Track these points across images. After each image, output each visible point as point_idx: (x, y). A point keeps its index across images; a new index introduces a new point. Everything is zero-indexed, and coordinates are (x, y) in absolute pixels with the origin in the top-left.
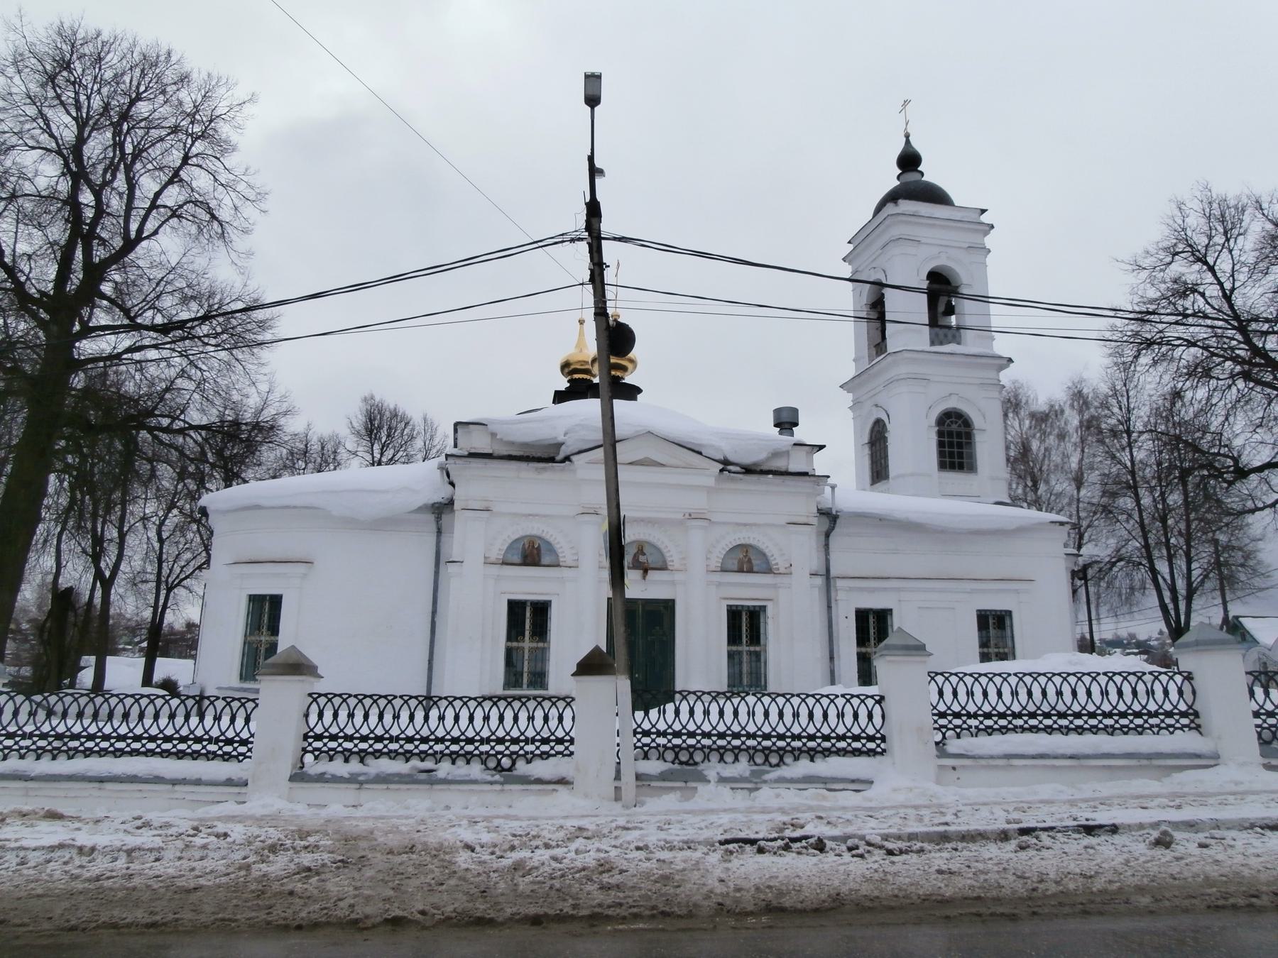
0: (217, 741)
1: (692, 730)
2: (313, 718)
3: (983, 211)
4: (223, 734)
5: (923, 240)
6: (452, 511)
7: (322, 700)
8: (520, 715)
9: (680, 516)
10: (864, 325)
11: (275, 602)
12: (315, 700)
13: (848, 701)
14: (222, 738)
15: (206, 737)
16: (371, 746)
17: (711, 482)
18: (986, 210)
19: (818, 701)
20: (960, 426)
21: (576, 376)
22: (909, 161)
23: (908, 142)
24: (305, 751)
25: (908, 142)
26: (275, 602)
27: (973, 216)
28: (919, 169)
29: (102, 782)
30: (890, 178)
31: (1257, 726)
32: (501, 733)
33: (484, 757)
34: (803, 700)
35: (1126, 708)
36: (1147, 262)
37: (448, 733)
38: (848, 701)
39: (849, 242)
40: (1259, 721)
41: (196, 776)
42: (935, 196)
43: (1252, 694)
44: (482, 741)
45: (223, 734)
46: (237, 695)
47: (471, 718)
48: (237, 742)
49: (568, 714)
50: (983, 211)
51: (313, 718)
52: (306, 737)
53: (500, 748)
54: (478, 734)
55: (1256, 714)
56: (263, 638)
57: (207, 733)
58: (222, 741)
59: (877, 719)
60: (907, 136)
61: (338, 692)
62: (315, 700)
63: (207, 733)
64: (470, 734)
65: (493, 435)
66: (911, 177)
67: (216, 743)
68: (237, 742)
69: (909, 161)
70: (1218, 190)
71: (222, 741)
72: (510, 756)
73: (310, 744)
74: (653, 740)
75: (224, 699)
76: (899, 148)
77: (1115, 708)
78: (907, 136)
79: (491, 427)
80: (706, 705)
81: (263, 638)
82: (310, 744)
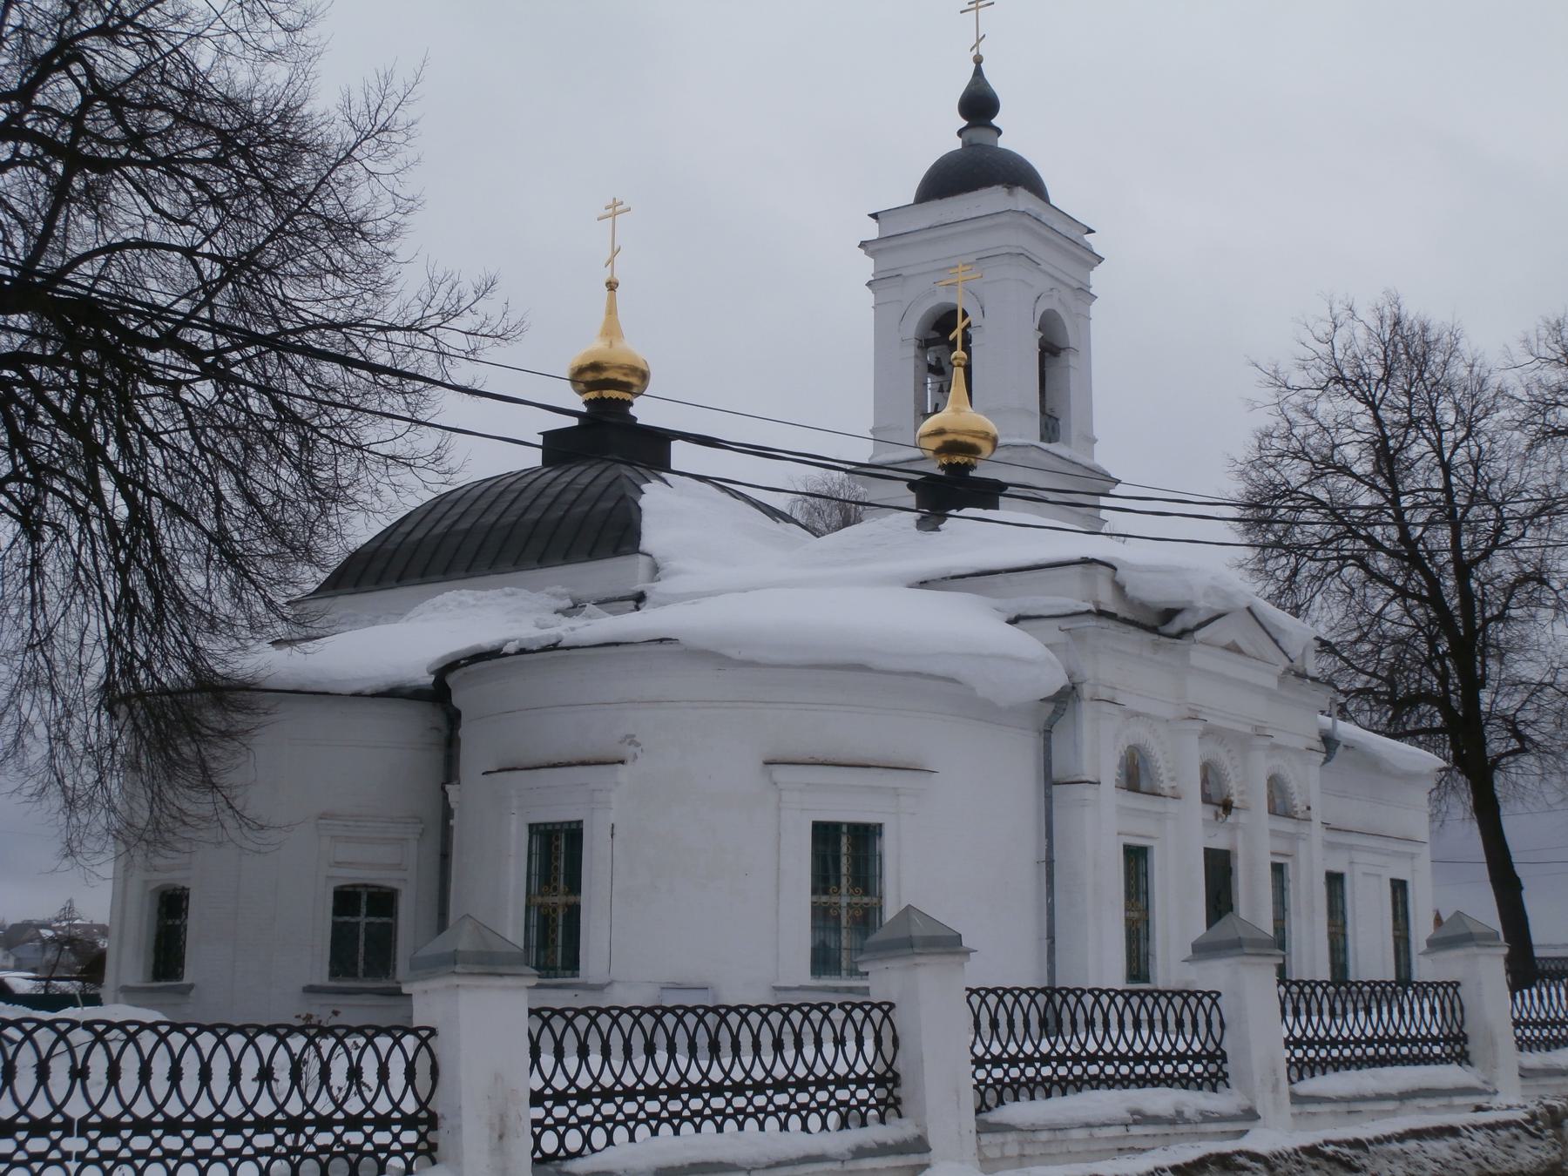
0: (84, 1127)
1: (325, 1113)
3: (1090, 231)
4: (95, 1110)
5: (1044, 266)
6: (1078, 698)
8: (333, 1065)
9: (1248, 730)
11: (865, 836)
14: (95, 1119)
15: (57, 1119)
17: (1271, 682)
18: (1093, 232)
21: (608, 394)
23: (978, 72)
25: (978, 72)
26: (865, 836)
27: (1073, 233)
28: (995, 122)
29: (1055, 1130)
31: (535, 1123)
36: (1296, 379)
39: (875, 216)
40: (538, 1113)
41: (802, 1154)
42: (1019, 176)
43: (535, 1053)
45: (95, 1110)
46: (815, 999)
48: (22, 1127)
49: (1516, 1015)
50: (1090, 231)
53: (382, 1138)
55: (536, 1099)
56: (844, 901)
57: (57, 1109)
58: (94, 1127)
60: (978, 61)
63: (57, 1109)
65: (1119, 588)
66: (980, 135)
67: (82, 1133)
68: (22, 1127)
70: (1413, 311)
71: (94, 1127)
74: (338, 1138)
75: (842, 1006)
76: (961, 81)
78: (978, 61)
79: (1122, 575)
80: (355, 1054)
81: (844, 901)
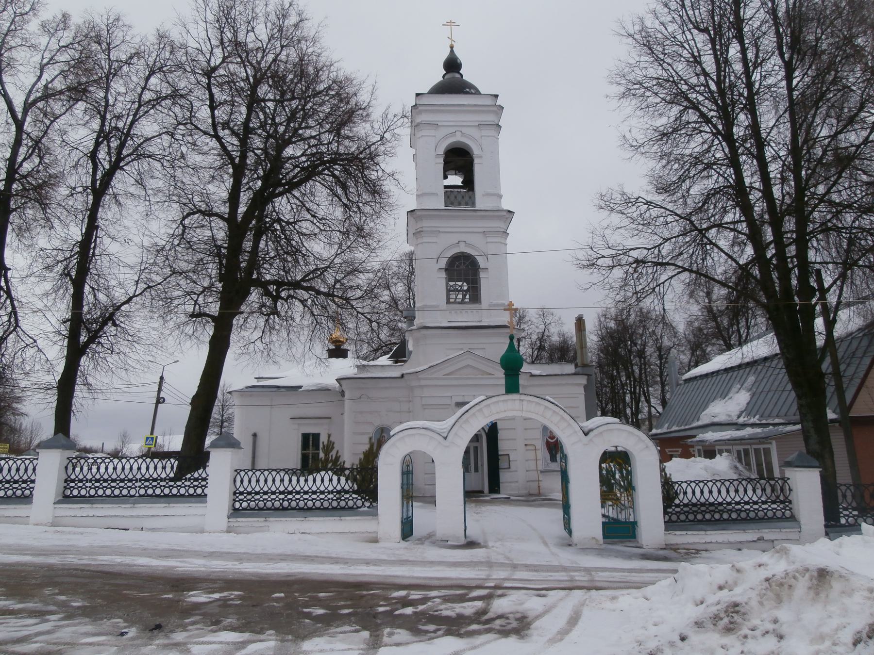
2: (238, 483)
7: (242, 473)
10: (664, 543)
12: (238, 473)
13: (689, 484)
16: (245, 497)
19: (697, 484)
20: (464, 263)
22: (452, 65)
23: (452, 51)
24: (234, 500)
25: (452, 51)
30: (437, 75)
32: (314, 489)
33: (330, 501)
34: (714, 483)
35: (740, 499)
37: (262, 489)
38: (689, 484)
44: (329, 492)
47: (274, 481)
51: (238, 483)
52: (235, 493)
54: (326, 489)
59: (238, 479)
60: (452, 47)
61: (693, 480)
62: (238, 473)
64: (273, 489)
69: (452, 65)
72: (288, 500)
73: (237, 497)
76: (446, 54)
77: (742, 499)
78: (452, 47)
82: (237, 497)
